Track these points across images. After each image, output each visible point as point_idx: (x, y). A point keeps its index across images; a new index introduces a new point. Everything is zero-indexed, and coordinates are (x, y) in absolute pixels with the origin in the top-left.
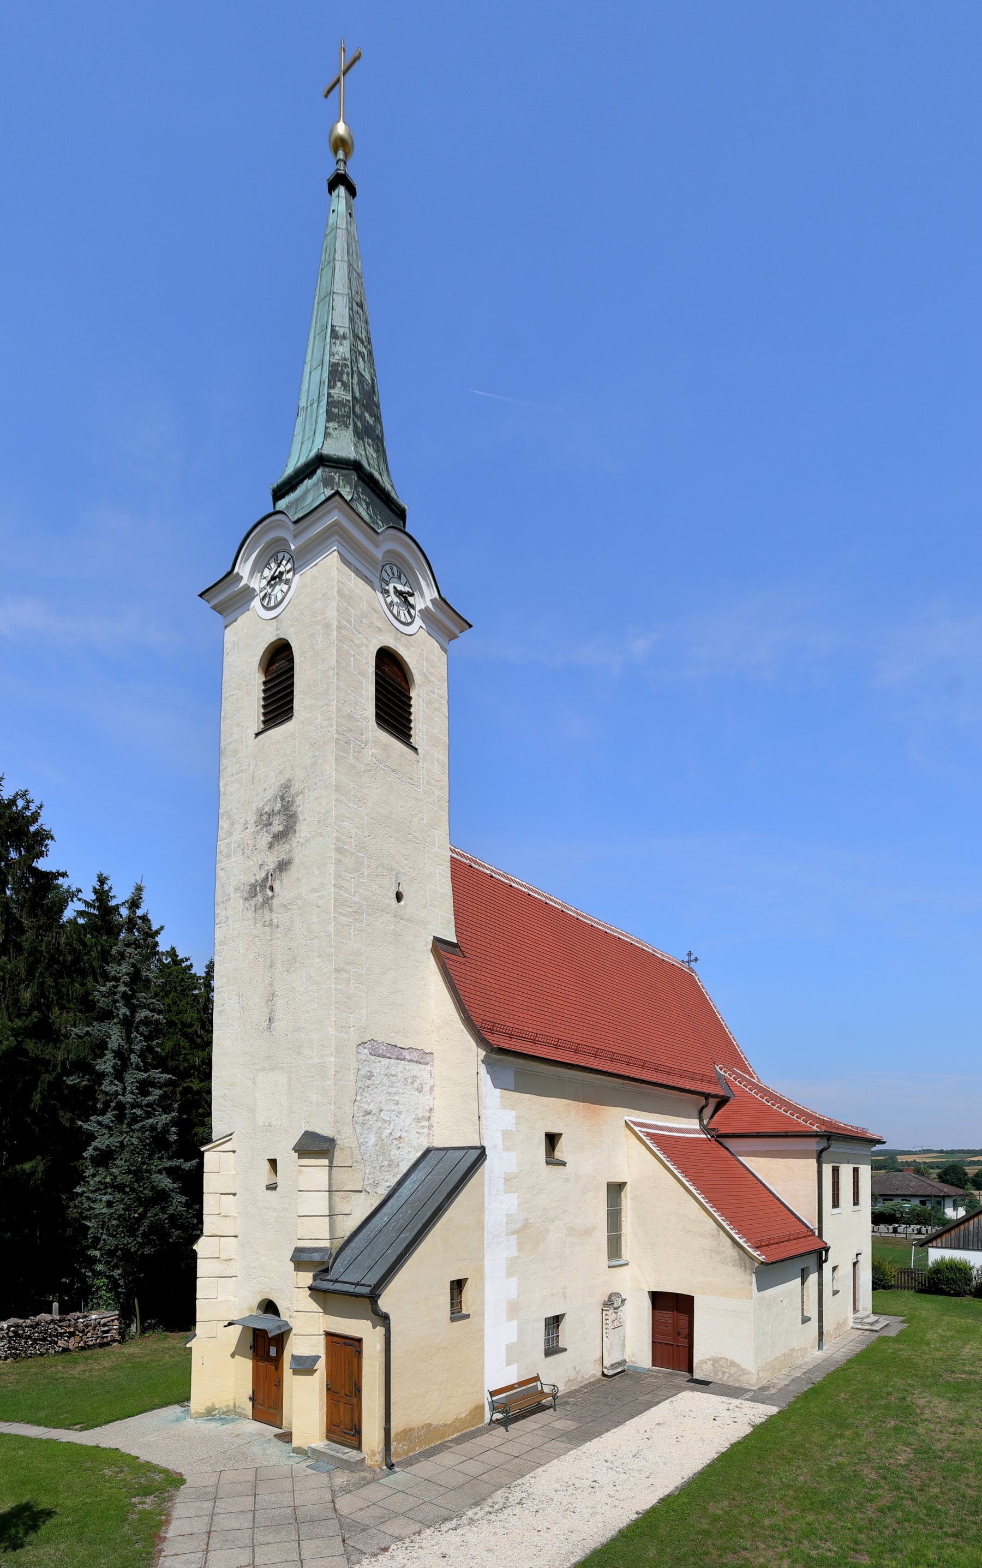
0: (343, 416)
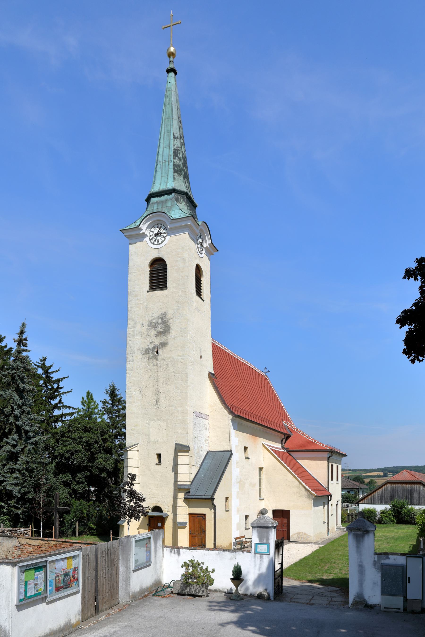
0: (179, 171)
